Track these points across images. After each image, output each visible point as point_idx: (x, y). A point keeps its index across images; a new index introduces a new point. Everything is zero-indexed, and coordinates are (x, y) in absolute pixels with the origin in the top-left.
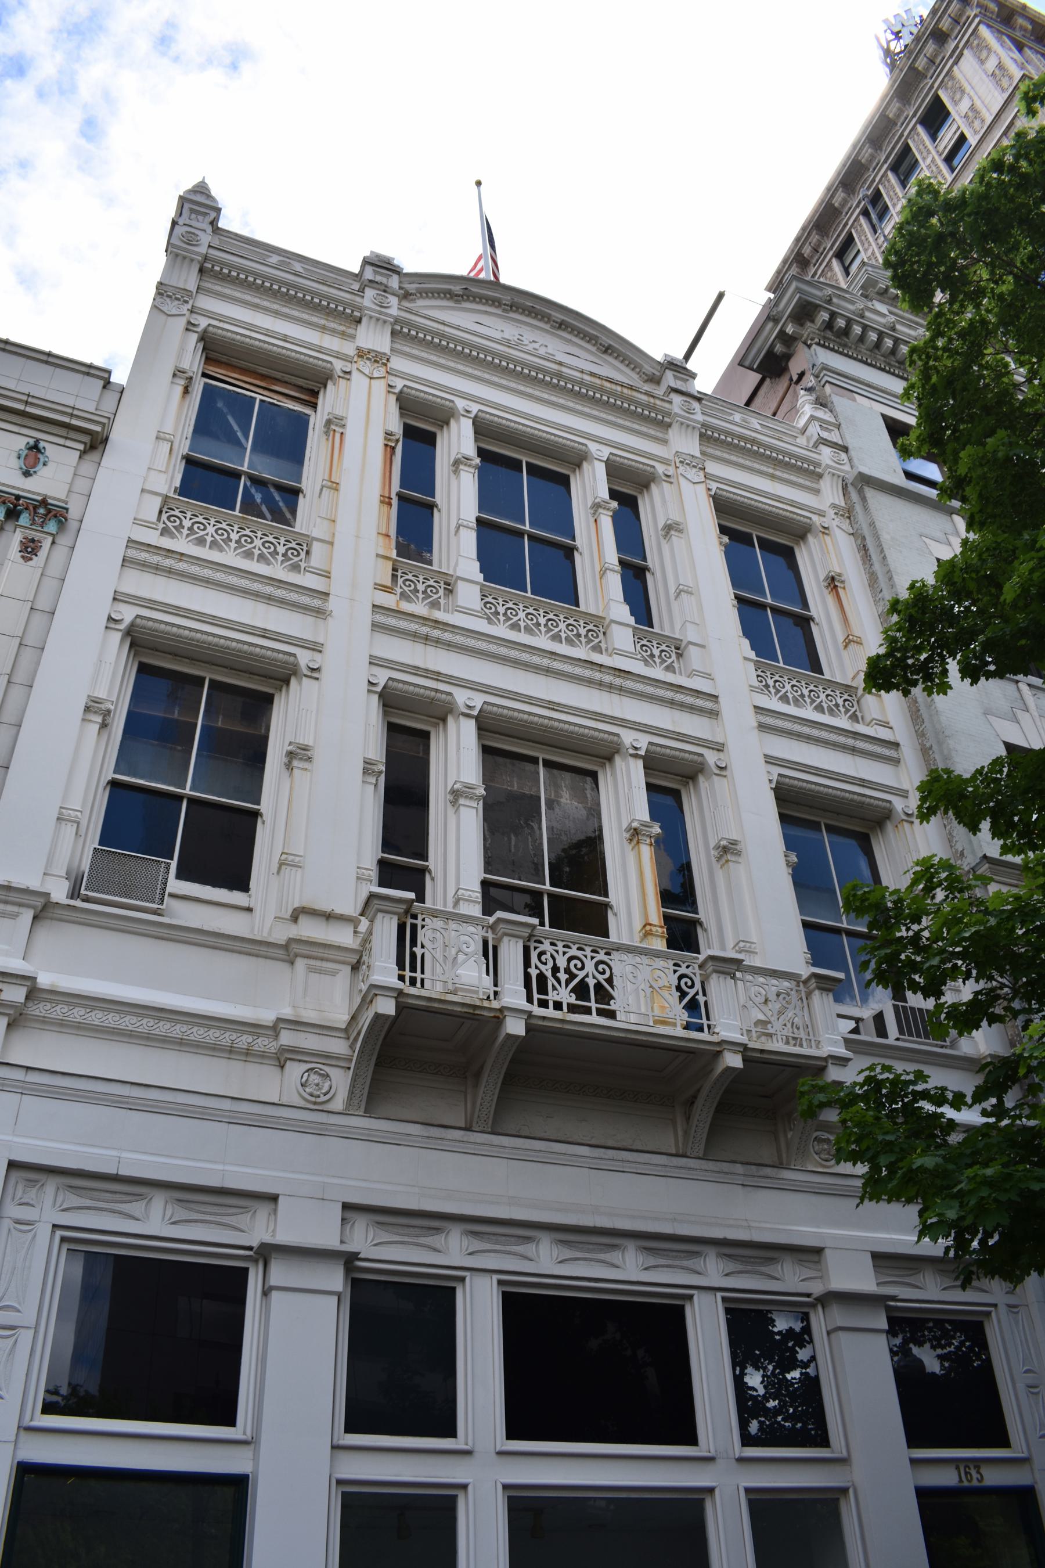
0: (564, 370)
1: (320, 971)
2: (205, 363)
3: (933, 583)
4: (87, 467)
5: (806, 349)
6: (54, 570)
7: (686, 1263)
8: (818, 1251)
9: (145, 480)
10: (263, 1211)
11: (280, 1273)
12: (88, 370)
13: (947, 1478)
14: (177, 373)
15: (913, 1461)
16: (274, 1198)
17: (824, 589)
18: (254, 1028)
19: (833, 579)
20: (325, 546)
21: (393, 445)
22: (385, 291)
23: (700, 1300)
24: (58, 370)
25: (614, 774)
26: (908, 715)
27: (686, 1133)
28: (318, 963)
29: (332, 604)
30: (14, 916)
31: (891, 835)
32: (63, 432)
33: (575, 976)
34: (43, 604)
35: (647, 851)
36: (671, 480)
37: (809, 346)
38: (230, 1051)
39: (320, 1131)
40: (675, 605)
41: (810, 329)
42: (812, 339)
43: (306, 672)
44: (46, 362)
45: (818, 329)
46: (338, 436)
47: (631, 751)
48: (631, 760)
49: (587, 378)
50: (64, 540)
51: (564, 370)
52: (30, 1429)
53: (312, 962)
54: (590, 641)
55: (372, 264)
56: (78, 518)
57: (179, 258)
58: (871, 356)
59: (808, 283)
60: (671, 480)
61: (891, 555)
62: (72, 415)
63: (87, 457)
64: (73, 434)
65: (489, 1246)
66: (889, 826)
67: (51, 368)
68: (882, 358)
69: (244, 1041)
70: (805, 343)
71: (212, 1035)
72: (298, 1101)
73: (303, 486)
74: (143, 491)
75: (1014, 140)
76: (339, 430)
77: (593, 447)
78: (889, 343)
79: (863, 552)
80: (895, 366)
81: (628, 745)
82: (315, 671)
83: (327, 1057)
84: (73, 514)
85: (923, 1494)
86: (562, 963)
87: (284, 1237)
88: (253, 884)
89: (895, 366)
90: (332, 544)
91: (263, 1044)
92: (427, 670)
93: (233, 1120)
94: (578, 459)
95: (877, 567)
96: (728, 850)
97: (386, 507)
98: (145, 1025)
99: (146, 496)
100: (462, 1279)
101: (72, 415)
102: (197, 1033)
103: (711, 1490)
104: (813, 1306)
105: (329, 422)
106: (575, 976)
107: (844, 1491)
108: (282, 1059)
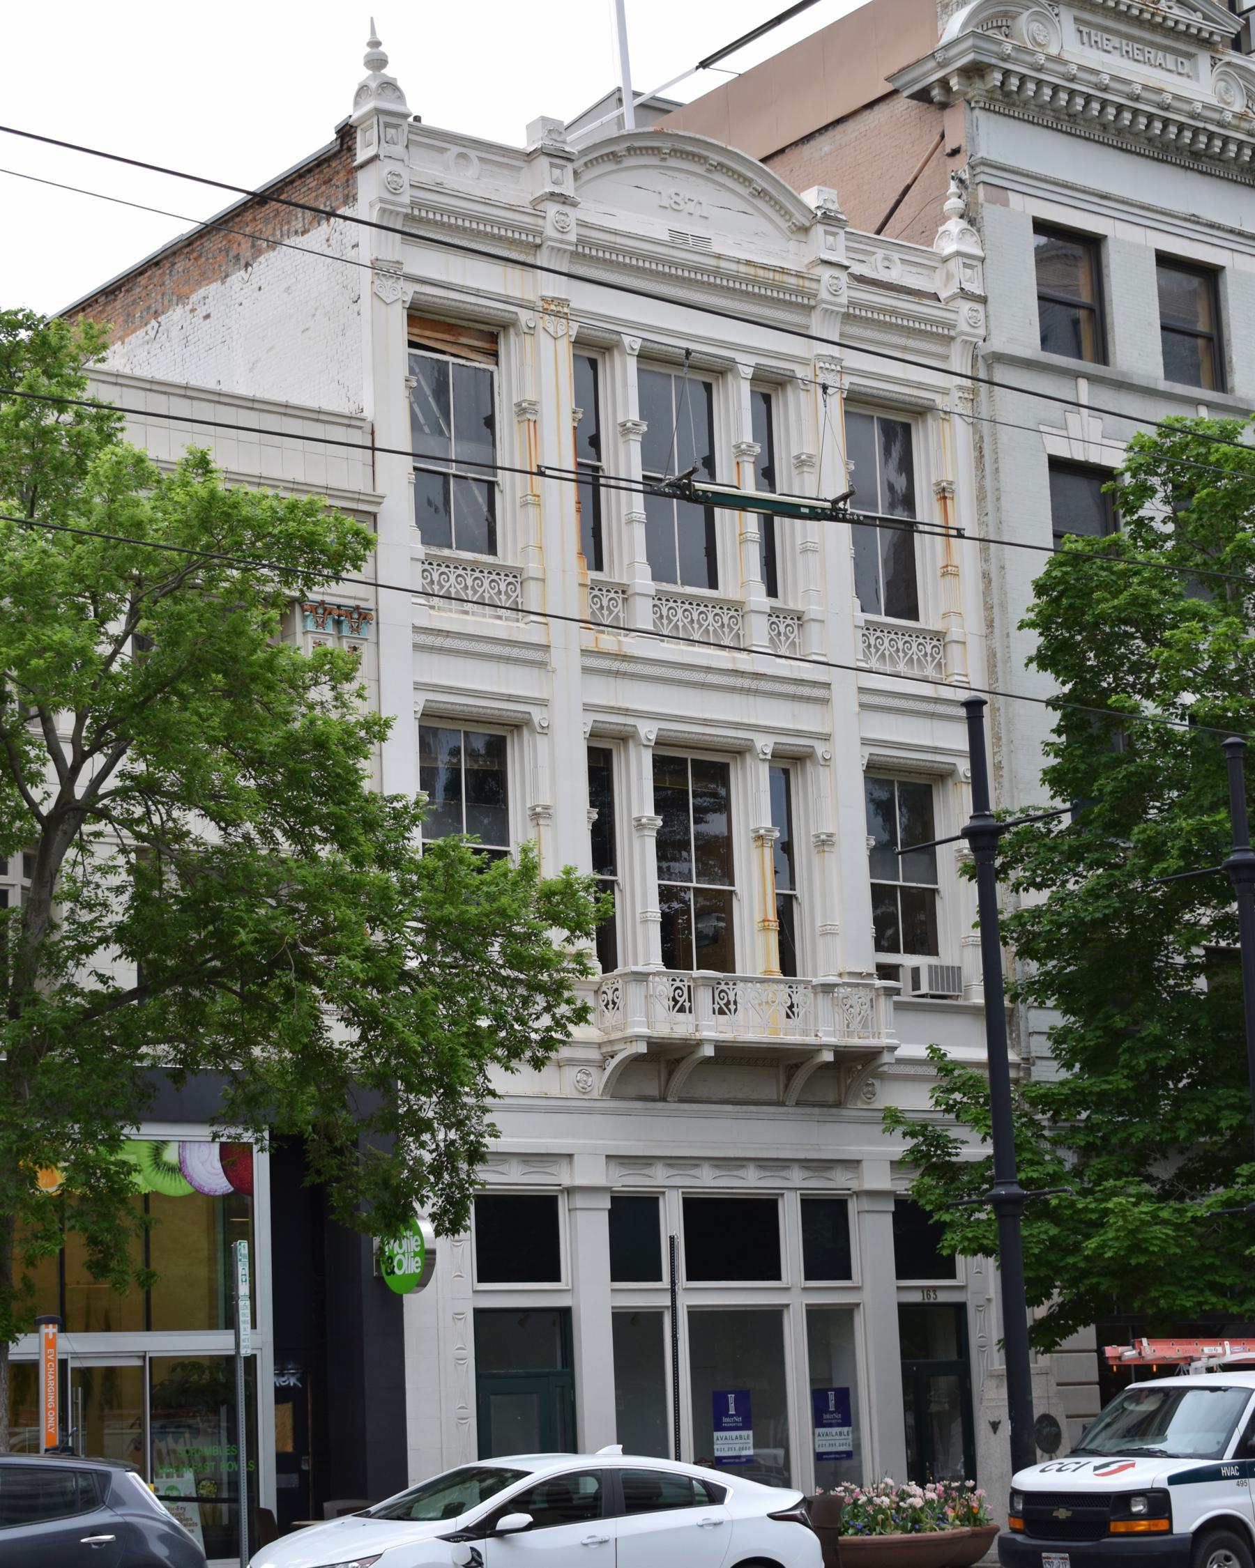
0: (723, 264)
5: (968, 111)
7: (781, 1174)
8: (859, 1162)
11: (579, 1201)
13: (916, 1297)
15: (899, 1288)
16: (570, 1156)
17: (933, 495)
19: (944, 490)
20: (540, 583)
22: (564, 203)
23: (787, 1194)
25: (744, 768)
26: (986, 664)
27: (786, 1087)
31: (950, 792)
35: (768, 853)
37: (972, 109)
40: (800, 559)
41: (978, 89)
43: (539, 730)
44: (317, 420)
46: (532, 424)
47: (762, 756)
48: (761, 764)
49: (743, 269)
51: (723, 264)
54: (731, 630)
57: (387, 213)
59: (967, 1203)
61: (1005, 465)
66: (950, 783)
70: (969, 102)
76: (532, 418)
77: (739, 357)
79: (977, 453)
81: (759, 750)
83: (588, 1062)
85: (903, 1308)
87: (579, 1181)
90: (543, 580)
92: (619, 709)
95: (988, 483)
96: (824, 843)
100: (663, 1193)
101: (358, 500)
103: (788, 1306)
104: (851, 1195)
107: (858, 1305)
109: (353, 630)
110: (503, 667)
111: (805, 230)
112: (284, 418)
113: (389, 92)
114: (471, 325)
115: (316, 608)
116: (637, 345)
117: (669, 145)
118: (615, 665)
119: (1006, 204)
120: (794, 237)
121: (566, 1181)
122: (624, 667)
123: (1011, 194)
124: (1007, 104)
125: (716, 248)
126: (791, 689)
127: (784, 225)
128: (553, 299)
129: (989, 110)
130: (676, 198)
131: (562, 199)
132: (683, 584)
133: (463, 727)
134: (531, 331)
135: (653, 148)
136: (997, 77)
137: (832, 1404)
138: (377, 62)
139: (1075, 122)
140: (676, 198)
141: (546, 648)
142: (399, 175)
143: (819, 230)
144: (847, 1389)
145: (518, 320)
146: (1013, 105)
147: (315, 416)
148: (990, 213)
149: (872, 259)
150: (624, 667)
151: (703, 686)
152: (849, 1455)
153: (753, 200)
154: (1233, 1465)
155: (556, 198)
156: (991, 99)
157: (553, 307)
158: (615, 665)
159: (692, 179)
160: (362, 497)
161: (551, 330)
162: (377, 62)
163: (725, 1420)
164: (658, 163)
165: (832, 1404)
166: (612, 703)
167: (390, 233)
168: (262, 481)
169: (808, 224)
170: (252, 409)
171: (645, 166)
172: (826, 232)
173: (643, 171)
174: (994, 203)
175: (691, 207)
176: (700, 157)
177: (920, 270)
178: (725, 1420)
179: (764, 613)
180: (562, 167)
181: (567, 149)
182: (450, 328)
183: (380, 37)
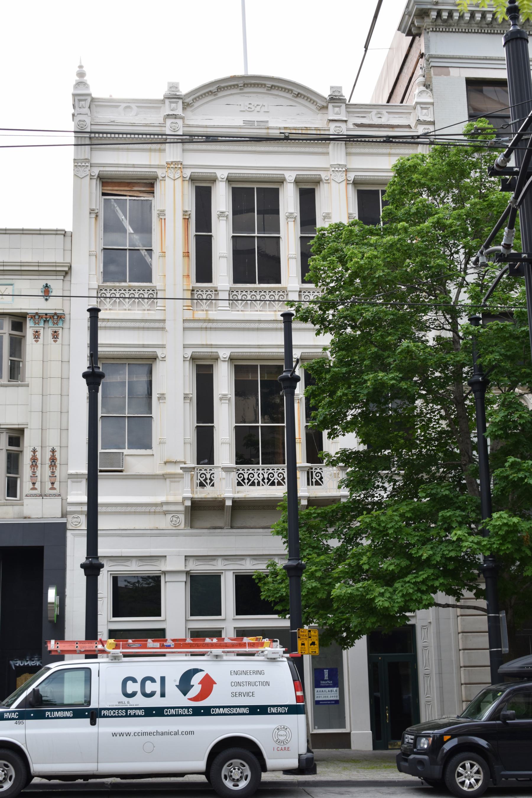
1: (174, 482)
2: (102, 186)
3: (507, 166)
4: (67, 283)
6: (66, 342)
9: (89, 284)
10: (163, 560)
11: (168, 578)
12: (56, 232)
14: (92, 211)
16: (166, 556)
18: (156, 505)
21: (188, 217)
22: (175, 118)
24: (45, 236)
28: (173, 479)
29: (168, 325)
30: (81, 482)
32: (54, 273)
33: (250, 480)
34: (65, 359)
36: (329, 181)
37: (428, 32)
38: (149, 513)
39: (177, 535)
41: (427, 22)
42: (429, 29)
44: (40, 234)
45: (432, 22)
46: (163, 221)
50: (66, 326)
52: (110, 622)
53: (171, 479)
55: (169, 98)
56: (68, 313)
58: (468, 26)
60: (329, 181)
62: (56, 266)
63: (66, 279)
64: (58, 273)
65: (230, 563)
67: (42, 236)
68: (476, 25)
69: (153, 509)
71: (143, 509)
72: (170, 527)
73: (153, 248)
74: (89, 289)
75: (330, 225)
78: (478, 16)
80: (485, 27)
82: (164, 359)
84: (66, 312)
86: (246, 476)
88: (153, 446)
89: (485, 27)
90: (165, 290)
91: (158, 509)
92: (207, 345)
93: (151, 536)
94: (282, 181)
97: (186, 259)
98: (123, 509)
99: (90, 290)
102: (139, 509)
105: (159, 215)
106: (250, 480)
108: (165, 513)
109: (54, 324)
110: (204, 332)
111: (326, 108)
112: (22, 235)
113: (81, 86)
114: (139, 181)
115: (34, 316)
116: (293, 179)
117: (242, 82)
118: (205, 325)
119: (448, 74)
120: (320, 112)
121: (164, 569)
122: (210, 325)
123: (450, 69)
124: (447, 26)
125: (270, 125)
126: (142, 325)
127: (313, 107)
128: (172, 163)
129: (436, 31)
130: (250, 106)
131: (174, 117)
132: (259, 283)
133: (127, 362)
134: (328, 182)
135: (234, 85)
136: (434, 14)
137: (326, 676)
138: (81, 74)
139: (492, 27)
140: (250, 106)
141: (164, 321)
142: (84, 121)
143: (330, 106)
144: (336, 669)
145: (216, 176)
146: (450, 26)
147: (38, 232)
148: (437, 81)
149: (370, 115)
150: (210, 325)
151: (258, 329)
152: (336, 702)
153: (295, 99)
154: (14, 712)
155: (171, 117)
156: (436, 25)
157: (172, 166)
158: (205, 325)
159: (260, 95)
160: (57, 264)
161: (172, 177)
162: (81, 74)
163: (321, 682)
164: (239, 91)
165: (326, 676)
166: (204, 343)
167: (83, 146)
168: (5, 264)
169: (325, 104)
170: (6, 234)
171: (231, 94)
172: (334, 106)
173: (232, 97)
174: (440, 75)
175: (258, 108)
176: (262, 85)
177: (401, 116)
178: (321, 682)
179: (296, 291)
180: (176, 103)
181: (178, 94)
182: (129, 184)
183: (83, 64)
